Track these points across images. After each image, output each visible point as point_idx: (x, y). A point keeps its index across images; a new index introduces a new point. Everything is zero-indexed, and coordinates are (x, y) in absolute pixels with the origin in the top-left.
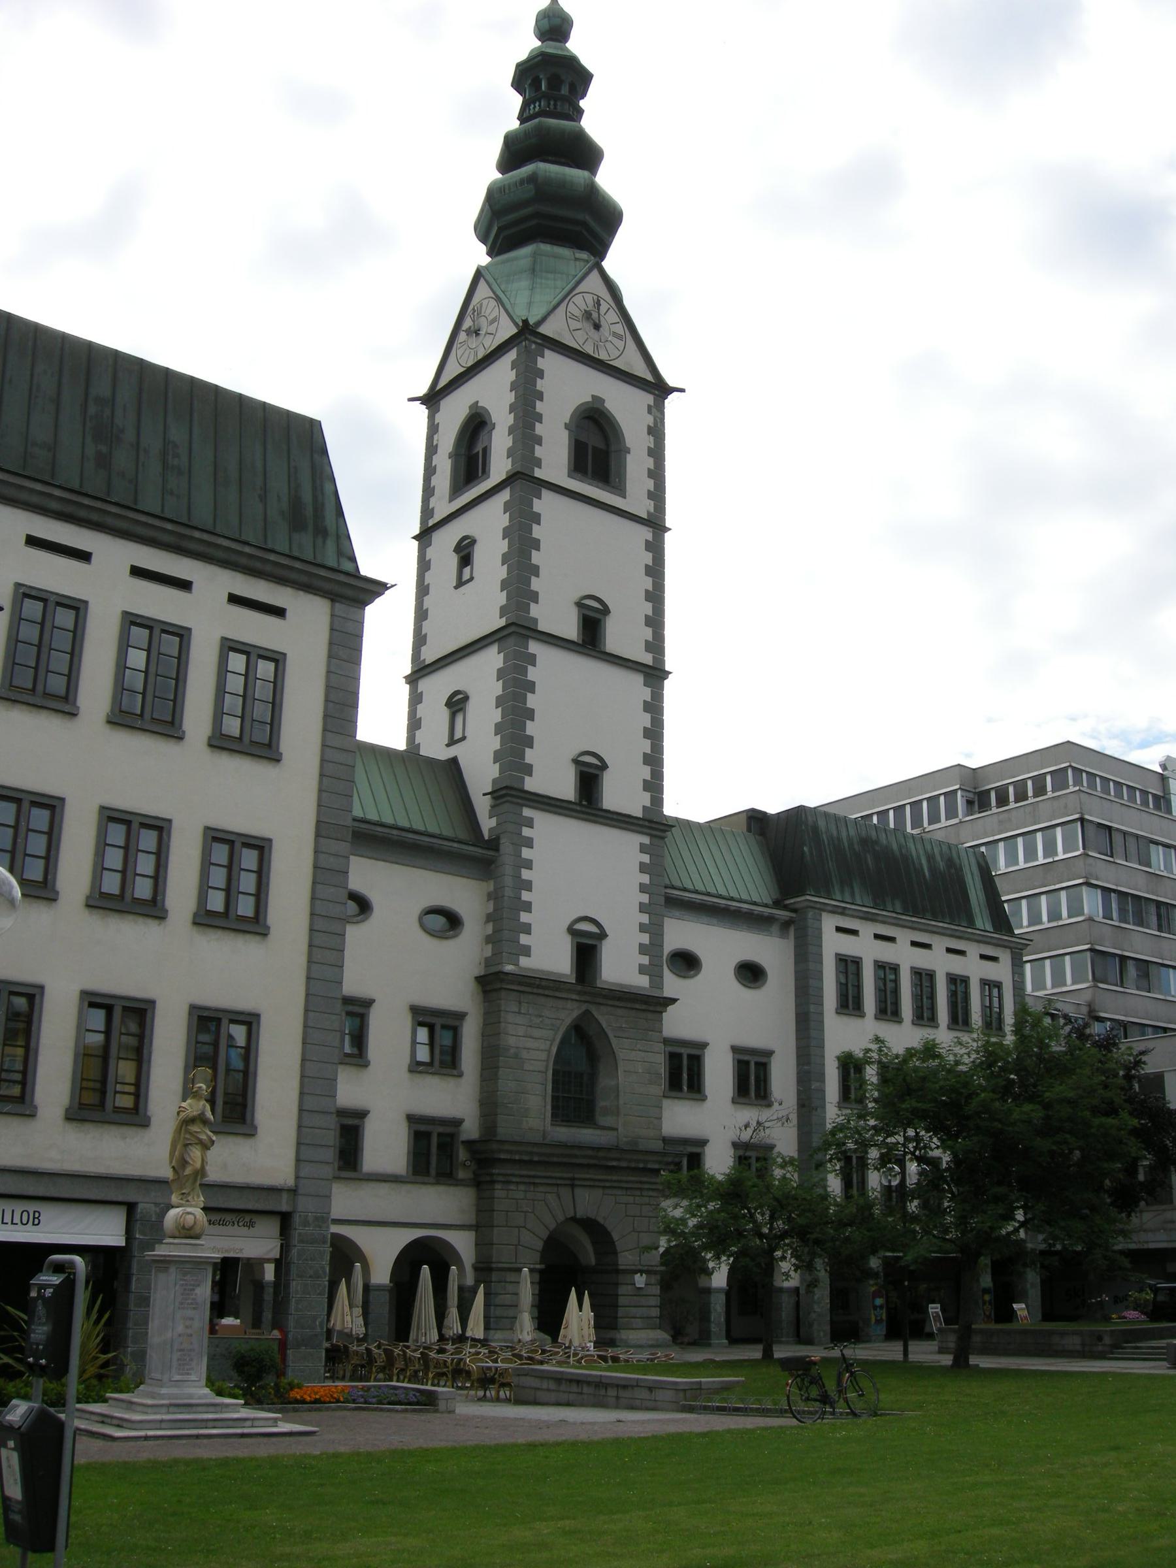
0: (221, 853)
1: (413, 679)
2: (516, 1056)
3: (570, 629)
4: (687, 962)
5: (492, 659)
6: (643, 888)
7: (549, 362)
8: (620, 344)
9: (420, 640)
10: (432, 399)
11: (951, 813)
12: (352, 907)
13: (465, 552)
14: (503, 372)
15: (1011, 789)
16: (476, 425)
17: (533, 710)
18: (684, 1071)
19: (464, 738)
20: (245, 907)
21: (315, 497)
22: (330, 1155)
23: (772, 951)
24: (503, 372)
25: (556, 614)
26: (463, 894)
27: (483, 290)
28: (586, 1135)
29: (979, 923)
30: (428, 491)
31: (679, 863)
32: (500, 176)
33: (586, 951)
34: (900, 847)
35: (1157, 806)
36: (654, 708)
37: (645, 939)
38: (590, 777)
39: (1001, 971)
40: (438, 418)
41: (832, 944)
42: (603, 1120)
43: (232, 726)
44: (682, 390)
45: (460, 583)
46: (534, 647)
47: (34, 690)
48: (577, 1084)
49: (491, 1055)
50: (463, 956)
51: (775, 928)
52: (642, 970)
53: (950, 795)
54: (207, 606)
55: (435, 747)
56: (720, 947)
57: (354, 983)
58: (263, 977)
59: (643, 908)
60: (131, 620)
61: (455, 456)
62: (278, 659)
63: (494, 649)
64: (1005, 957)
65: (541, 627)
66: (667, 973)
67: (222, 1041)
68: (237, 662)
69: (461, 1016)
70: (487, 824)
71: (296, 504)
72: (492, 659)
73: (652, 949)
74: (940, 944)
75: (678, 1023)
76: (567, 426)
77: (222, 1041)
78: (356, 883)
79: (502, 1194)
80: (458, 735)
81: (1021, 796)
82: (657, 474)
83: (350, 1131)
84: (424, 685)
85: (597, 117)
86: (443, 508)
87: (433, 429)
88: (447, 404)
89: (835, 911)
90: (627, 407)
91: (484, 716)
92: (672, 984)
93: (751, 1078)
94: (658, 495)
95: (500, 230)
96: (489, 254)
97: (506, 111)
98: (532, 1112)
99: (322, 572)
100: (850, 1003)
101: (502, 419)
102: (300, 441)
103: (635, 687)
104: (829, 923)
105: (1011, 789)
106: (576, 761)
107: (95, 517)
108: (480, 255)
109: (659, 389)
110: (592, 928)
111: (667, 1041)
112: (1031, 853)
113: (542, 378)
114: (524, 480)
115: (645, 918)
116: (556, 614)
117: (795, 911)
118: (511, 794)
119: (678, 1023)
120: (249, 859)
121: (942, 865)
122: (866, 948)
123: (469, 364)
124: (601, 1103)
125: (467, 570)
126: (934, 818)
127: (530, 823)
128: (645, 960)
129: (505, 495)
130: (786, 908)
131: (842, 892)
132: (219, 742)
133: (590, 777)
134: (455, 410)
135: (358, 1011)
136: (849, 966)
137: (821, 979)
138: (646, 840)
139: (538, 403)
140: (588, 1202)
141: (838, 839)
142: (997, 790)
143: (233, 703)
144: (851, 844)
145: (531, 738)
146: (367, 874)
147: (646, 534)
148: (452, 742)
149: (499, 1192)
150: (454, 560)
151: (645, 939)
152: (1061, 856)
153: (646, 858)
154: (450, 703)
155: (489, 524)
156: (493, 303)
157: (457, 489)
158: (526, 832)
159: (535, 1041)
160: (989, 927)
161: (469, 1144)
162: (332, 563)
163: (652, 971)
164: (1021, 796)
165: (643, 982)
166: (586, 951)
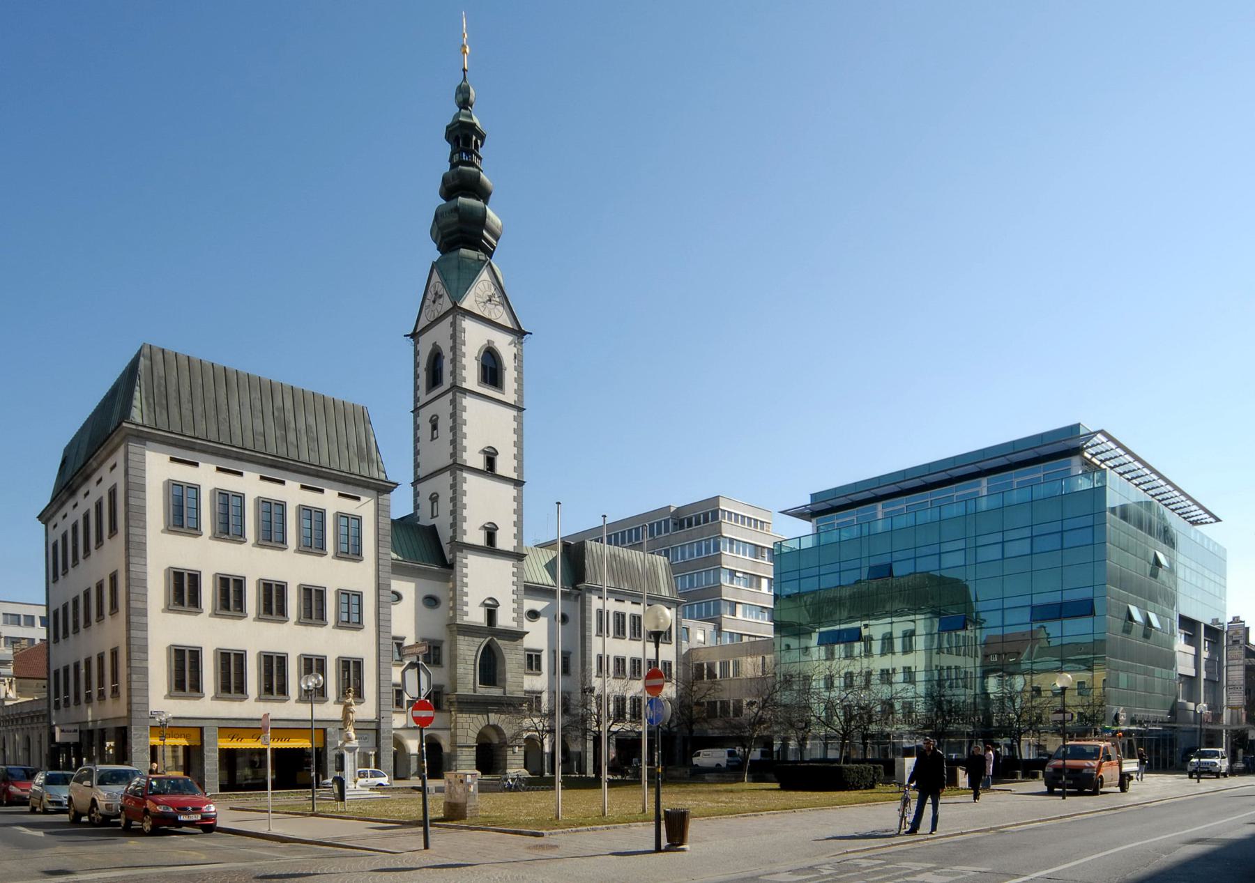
0: (344, 599)
1: (414, 484)
3: (480, 463)
4: (534, 615)
7: (468, 324)
9: (417, 466)
10: (415, 335)
11: (667, 530)
14: (445, 327)
20: (355, 618)
28: (495, 692)
32: (444, 202)
33: (491, 615)
37: (515, 606)
38: (491, 533)
45: (433, 439)
50: (436, 619)
53: (666, 521)
55: (425, 520)
57: (396, 631)
58: (360, 644)
61: (427, 370)
62: (359, 519)
68: (344, 522)
70: (449, 557)
72: (446, 478)
73: (518, 610)
75: (528, 642)
84: (420, 487)
87: (417, 353)
90: (504, 345)
91: (445, 505)
92: (527, 625)
103: (510, 490)
112: (699, 553)
114: (458, 389)
119: (528, 642)
120: (355, 600)
126: (659, 533)
129: (450, 396)
140: (494, 718)
148: (433, 517)
150: (429, 426)
159: (469, 651)
162: (376, 476)
163: (518, 619)
165: (515, 624)
166: (491, 615)
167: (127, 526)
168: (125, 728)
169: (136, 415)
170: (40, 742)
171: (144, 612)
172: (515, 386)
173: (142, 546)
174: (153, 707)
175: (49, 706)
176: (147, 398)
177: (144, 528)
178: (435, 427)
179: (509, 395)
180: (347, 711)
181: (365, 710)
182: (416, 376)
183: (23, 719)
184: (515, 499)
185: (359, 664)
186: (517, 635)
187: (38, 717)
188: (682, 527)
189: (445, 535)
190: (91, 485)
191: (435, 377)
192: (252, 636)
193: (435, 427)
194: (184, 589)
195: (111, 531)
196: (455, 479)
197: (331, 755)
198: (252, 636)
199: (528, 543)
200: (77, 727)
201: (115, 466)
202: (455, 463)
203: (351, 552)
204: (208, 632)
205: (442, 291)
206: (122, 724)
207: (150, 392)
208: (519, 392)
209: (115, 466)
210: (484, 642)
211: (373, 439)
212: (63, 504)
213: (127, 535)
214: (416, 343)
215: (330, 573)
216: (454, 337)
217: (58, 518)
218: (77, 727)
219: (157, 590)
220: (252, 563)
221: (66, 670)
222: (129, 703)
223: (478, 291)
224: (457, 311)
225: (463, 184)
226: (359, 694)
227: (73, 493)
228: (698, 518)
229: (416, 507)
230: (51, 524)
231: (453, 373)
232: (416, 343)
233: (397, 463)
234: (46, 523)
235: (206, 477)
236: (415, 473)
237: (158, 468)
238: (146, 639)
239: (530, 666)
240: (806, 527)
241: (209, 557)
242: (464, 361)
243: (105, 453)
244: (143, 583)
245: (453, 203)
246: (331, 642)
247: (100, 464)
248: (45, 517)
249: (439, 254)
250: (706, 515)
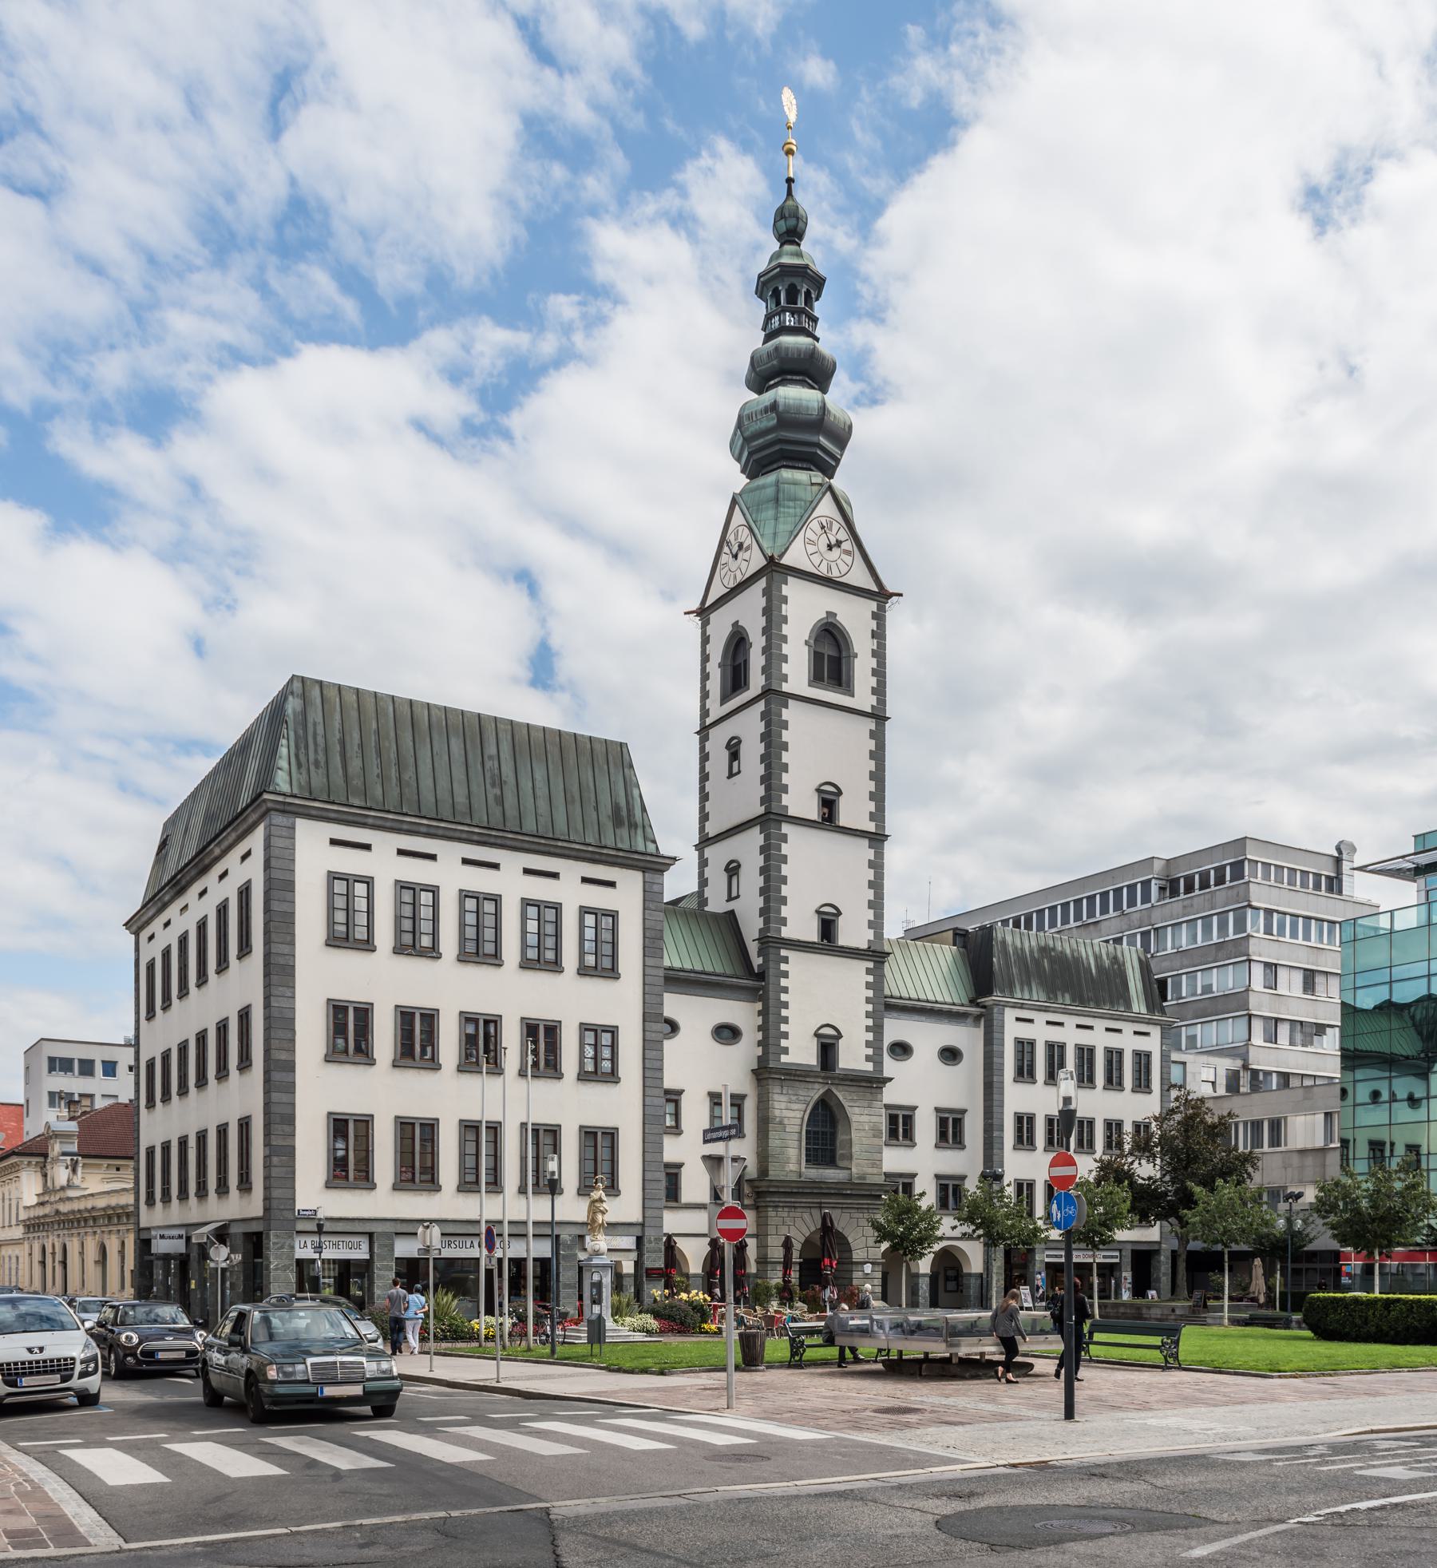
0: (590, 1038)
2: (781, 1123)
3: (813, 812)
4: (902, 1050)
5: (754, 838)
6: (868, 1000)
8: (848, 559)
9: (704, 817)
10: (704, 612)
12: (668, 1028)
13: (734, 750)
14: (754, 598)
15: (1197, 877)
16: (738, 642)
18: (900, 1126)
19: (738, 897)
21: (628, 803)
22: (662, 1194)
23: (967, 1038)
24: (754, 598)
25: (800, 801)
26: (741, 1013)
27: (738, 518)
28: (831, 1174)
29: (1135, 1008)
31: (898, 976)
33: (828, 1049)
34: (1072, 951)
35: (1330, 889)
36: (877, 865)
37: (870, 1036)
39: (1152, 1044)
41: (1012, 1030)
42: (840, 1164)
43: (590, 960)
45: (731, 775)
46: (786, 828)
47: (477, 953)
48: (825, 1133)
49: (764, 1122)
50: (740, 1058)
51: (970, 1020)
52: (868, 1058)
54: (570, 888)
55: (717, 903)
56: (927, 1037)
58: (620, 1107)
59: (868, 1015)
60: (526, 903)
62: (614, 915)
63: (757, 829)
64: (1156, 1032)
66: (886, 1058)
67: (599, 1144)
69: (743, 1097)
70: (757, 961)
71: (616, 809)
72: (754, 838)
73: (875, 1044)
74: (1100, 1025)
75: (892, 1095)
76: (806, 643)
77: (599, 1144)
78: (668, 1012)
79: (773, 1214)
80: (734, 894)
81: (1205, 885)
83: (673, 1174)
86: (716, 711)
87: (705, 640)
89: (1014, 1006)
90: (855, 617)
91: (751, 881)
93: (950, 1129)
95: (750, 454)
98: (791, 1161)
99: (636, 856)
100: (1025, 1072)
102: (613, 758)
103: (863, 851)
104: (1010, 1015)
105: (1197, 877)
106: (818, 912)
107: (499, 841)
109: (881, 596)
110: (833, 1032)
111: (887, 1107)
114: (774, 696)
115: (870, 1022)
116: (800, 801)
117: (984, 1007)
118: (771, 942)
119: (892, 1095)
121: (1107, 963)
122: (1040, 1032)
123: (732, 585)
124: (839, 1152)
125: (735, 764)
126: (1132, 903)
127: (786, 960)
128: (870, 1051)
129: (761, 706)
130: (978, 1005)
131: (1022, 991)
132: (583, 971)
133: (828, 925)
134: (721, 625)
135: (674, 1097)
136: (1025, 1048)
137: (1002, 1057)
138: (871, 965)
141: (1022, 949)
142: (1186, 878)
143: (589, 946)
144: (1031, 951)
145: (785, 898)
146: (674, 1005)
147: (871, 724)
148: (730, 899)
149: (771, 1213)
150: (726, 754)
151: (870, 1036)
152: (1231, 937)
153: (870, 979)
154: (727, 869)
155: (749, 726)
156: (747, 531)
157: (724, 699)
158: (783, 967)
159: (792, 1111)
160: (1144, 1010)
161: (749, 1181)
162: (641, 848)
163: (876, 1059)
164: (1205, 885)
165: (869, 1067)
166: (828, 1049)
167: (267, 942)
168: (259, 1235)
169: (282, 781)
170: (122, 1253)
171: (290, 1067)
172: (873, 663)
173: (289, 971)
174: (301, 1204)
175: (137, 1200)
176: (297, 756)
177: (292, 943)
178: (734, 756)
179: (863, 699)
180: (594, 1208)
181: (626, 1206)
182: (705, 676)
183: (95, 1219)
184: (871, 904)
185: (612, 1134)
186: (873, 1083)
187: (119, 1216)
188: (1174, 892)
189: (751, 926)
190: (210, 880)
191: (736, 678)
192: (448, 1096)
193: (734, 756)
194: (349, 1030)
195: (241, 949)
197: (568, 1276)
198: (448, 1096)
199: (893, 930)
200: (182, 1232)
201: (248, 854)
202: (768, 813)
203: (602, 965)
204: (383, 1093)
205: (745, 536)
206: (255, 1227)
207: (301, 743)
208: (880, 691)
209: (248, 854)
210: (816, 1092)
211: (636, 792)
212: (165, 906)
213: (267, 956)
214: (705, 624)
215: (568, 1000)
216: (767, 612)
217: (156, 926)
218: (182, 1232)
219: (311, 1031)
220: (450, 989)
221: (166, 1147)
222: (267, 1199)
223: (810, 534)
225: (786, 365)
226: (613, 1189)
227: (181, 891)
228: (1205, 876)
229: (703, 882)
230: (144, 935)
232: (705, 624)
233: (672, 814)
234: (137, 934)
235: (384, 861)
236: (702, 829)
237: (315, 851)
238: (293, 1105)
239: (893, 1133)
240: (1408, 892)
241: (385, 981)
243: (234, 836)
245: (768, 397)
246: (569, 1104)
247: (225, 852)
248: (136, 925)
249: (743, 480)
250: (1220, 871)
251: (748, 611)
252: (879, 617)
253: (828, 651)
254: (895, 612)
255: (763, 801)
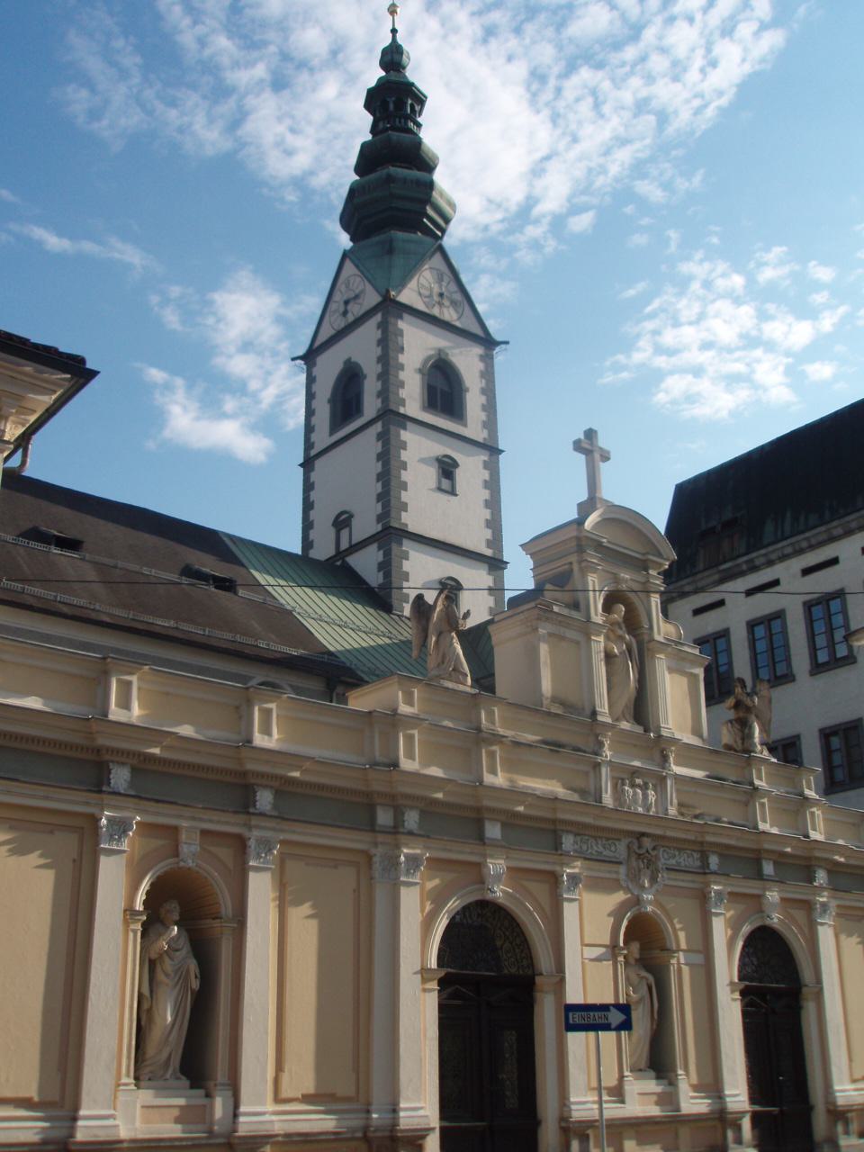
10: (310, 357)
14: (370, 330)
16: (350, 380)
17: (406, 504)
24: (370, 330)
30: (309, 429)
34: (37, 1133)
40: (316, 371)
44: (507, 343)
63: (374, 547)
65: (411, 529)
82: (490, 408)
85: (433, 131)
87: (311, 380)
88: (322, 360)
90: (467, 361)
94: (491, 424)
96: (352, 240)
97: (360, 126)
101: (371, 369)
108: (345, 241)
109: (488, 342)
113: (406, 490)
114: (391, 417)
129: (378, 427)
134: (329, 367)
139: (403, 514)
143: (762, 660)
147: (483, 457)
157: (336, 424)
196: (387, 554)
211: (655, 1027)
223: (422, 281)
224: (390, 308)
231: (384, 394)
242: (402, 375)
244: (291, 1104)
251: (361, 347)
252: (488, 359)
253: (440, 384)
254: (500, 356)
255: (380, 518)
